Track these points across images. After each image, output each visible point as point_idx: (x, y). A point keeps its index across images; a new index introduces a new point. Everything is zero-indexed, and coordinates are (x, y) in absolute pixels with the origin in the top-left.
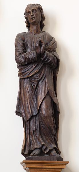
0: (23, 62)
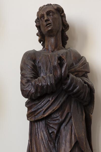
0: (33, 93)
